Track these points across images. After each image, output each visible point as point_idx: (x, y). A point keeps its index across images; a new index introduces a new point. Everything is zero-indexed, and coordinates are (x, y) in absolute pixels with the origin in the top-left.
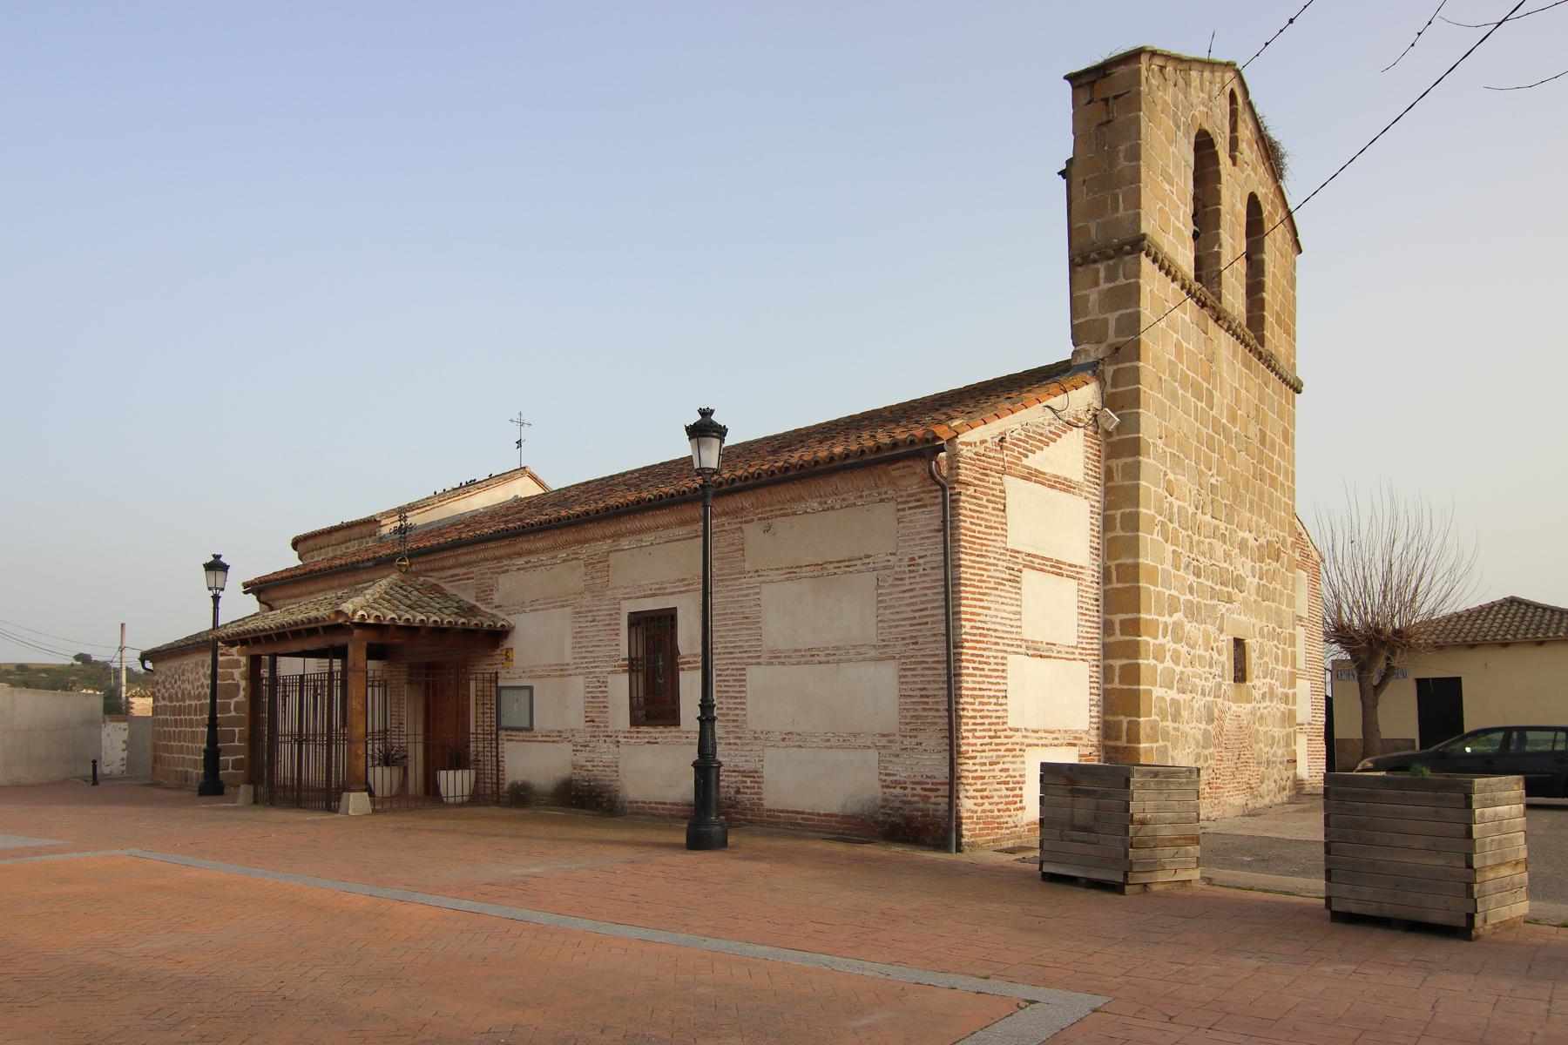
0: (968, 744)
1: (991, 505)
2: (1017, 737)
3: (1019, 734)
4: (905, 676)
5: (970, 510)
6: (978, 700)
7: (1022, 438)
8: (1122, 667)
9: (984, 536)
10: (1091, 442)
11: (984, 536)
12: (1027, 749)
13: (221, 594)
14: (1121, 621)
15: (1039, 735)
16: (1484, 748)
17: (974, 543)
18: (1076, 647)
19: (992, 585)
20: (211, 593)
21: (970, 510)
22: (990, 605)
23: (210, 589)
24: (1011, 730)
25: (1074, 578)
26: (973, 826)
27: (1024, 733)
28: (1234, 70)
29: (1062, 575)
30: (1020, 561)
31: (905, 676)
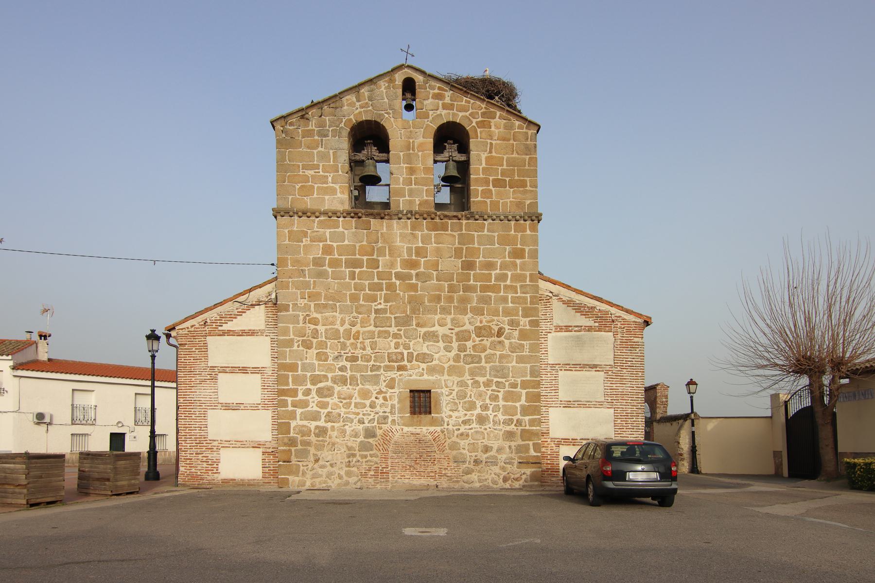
0: (182, 446)
1: (197, 350)
2: (215, 444)
3: (217, 442)
4: (545, 351)
5: (184, 354)
6: (187, 429)
7: (218, 319)
8: (527, 376)
9: (192, 364)
10: (271, 309)
11: (192, 364)
12: (222, 449)
13: (156, 354)
14: (328, 381)
15: (231, 442)
16: (719, 479)
17: (186, 367)
18: (260, 404)
19: (198, 383)
20: (150, 354)
21: (184, 354)
22: (196, 391)
23: (149, 351)
24: (210, 440)
25: (258, 373)
26: (184, 477)
27: (220, 442)
28: (406, 67)
29: (248, 373)
30: (216, 370)
31: (545, 351)
